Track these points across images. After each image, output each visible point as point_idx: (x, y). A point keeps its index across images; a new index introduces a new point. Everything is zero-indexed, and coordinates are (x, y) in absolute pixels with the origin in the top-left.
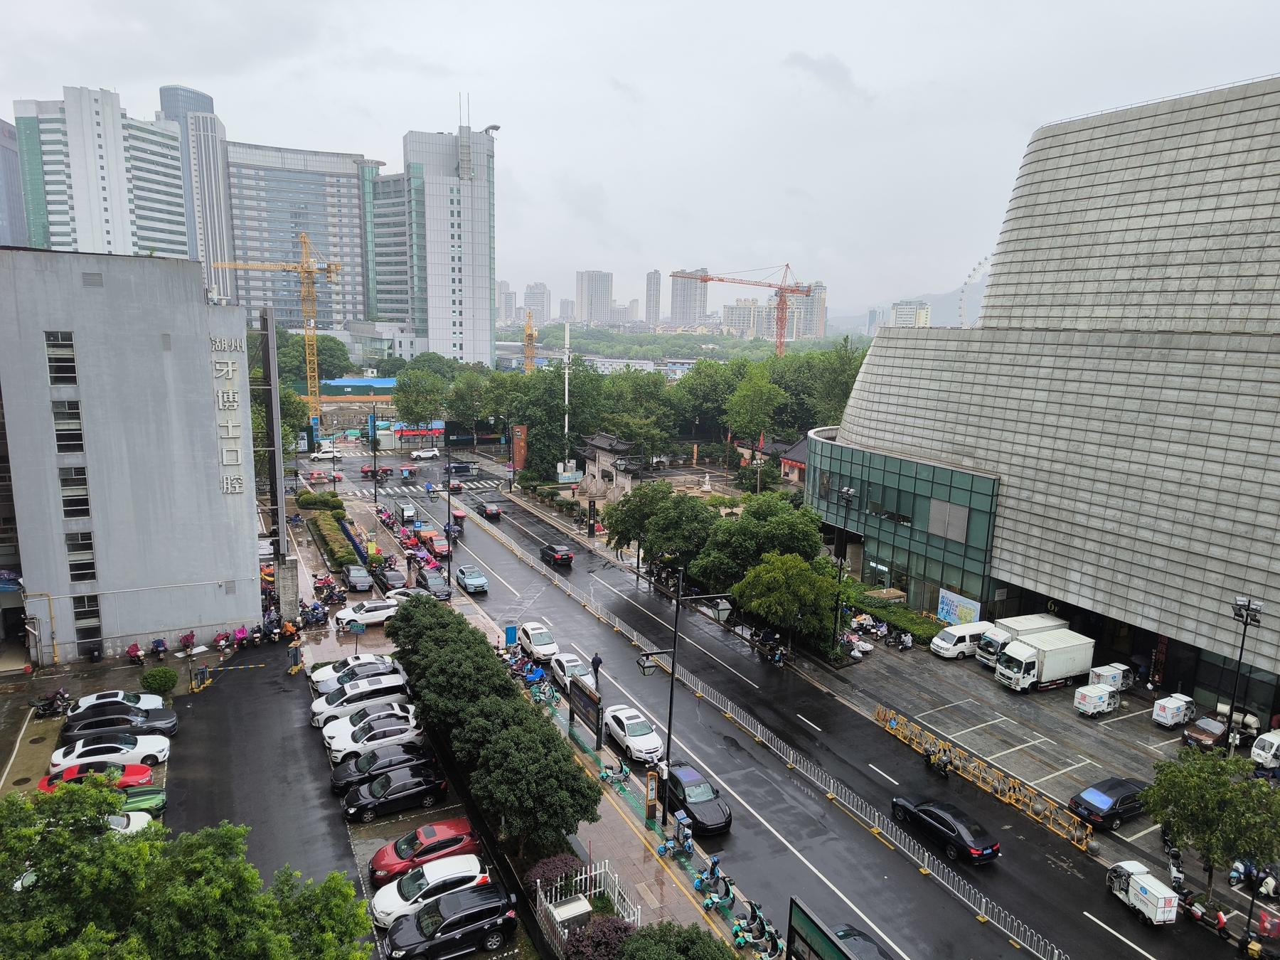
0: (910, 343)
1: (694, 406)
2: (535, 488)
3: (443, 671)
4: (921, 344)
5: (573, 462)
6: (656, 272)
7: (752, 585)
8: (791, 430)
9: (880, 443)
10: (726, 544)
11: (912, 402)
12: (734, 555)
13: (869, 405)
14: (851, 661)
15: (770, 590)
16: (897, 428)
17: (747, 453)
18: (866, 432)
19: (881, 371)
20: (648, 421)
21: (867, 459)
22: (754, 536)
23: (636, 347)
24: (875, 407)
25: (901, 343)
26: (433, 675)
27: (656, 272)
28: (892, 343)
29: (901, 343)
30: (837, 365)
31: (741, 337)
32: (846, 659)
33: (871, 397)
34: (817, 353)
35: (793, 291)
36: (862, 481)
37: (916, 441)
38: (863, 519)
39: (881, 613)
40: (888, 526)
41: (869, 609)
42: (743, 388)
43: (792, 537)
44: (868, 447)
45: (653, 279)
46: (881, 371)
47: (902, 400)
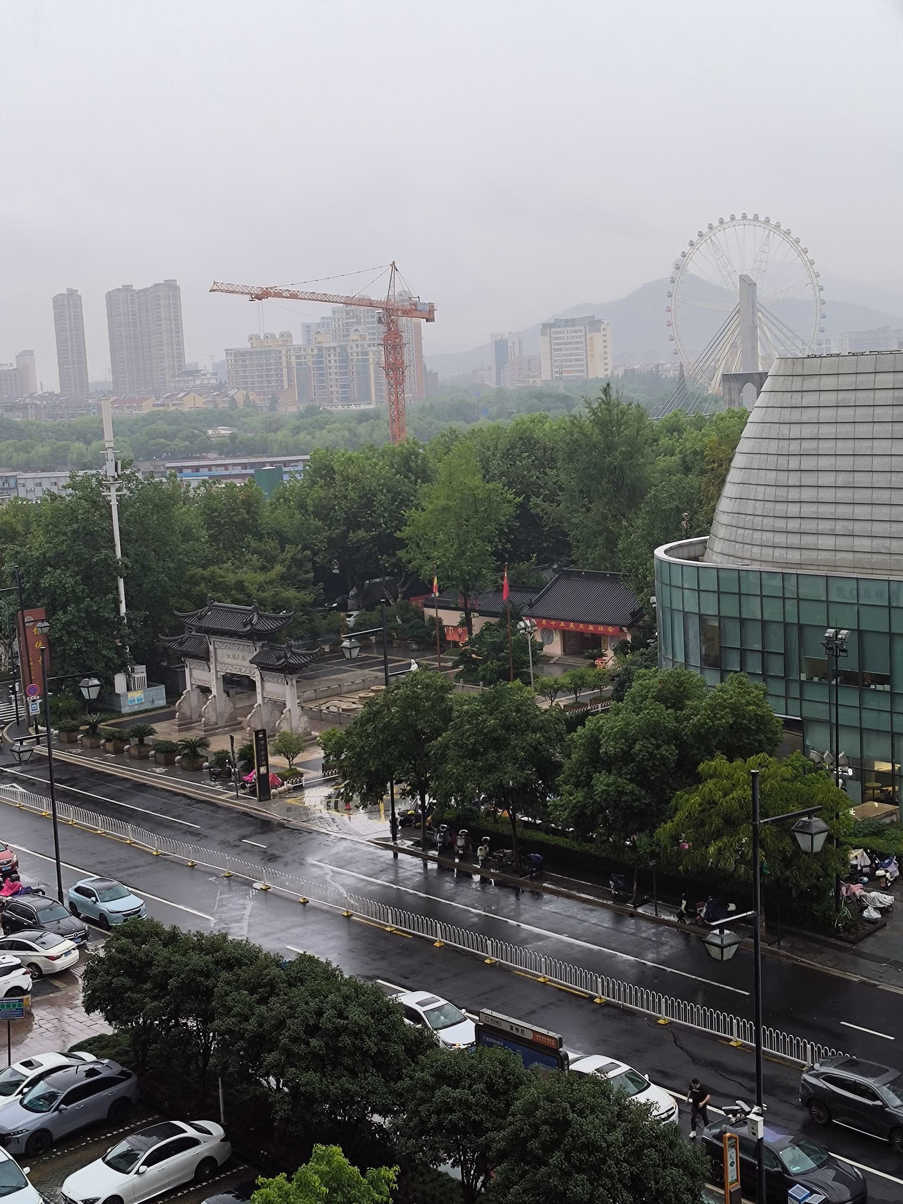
0: (846, 382)
1: (330, 540)
2: (94, 726)
3: (313, 1030)
4: (865, 381)
5: (140, 672)
6: (72, 293)
7: (698, 822)
8: (524, 566)
9: (813, 555)
10: (626, 757)
11: (862, 479)
12: (641, 777)
13: (781, 493)
14: (869, 927)
15: (730, 823)
16: (840, 527)
17: (451, 618)
18: (780, 539)
19: (795, 431)
20: (273, 574)
21: (787, 585)
22: (675, 737)
23: (78, 445)
24: (793, 494)
25: (829, 383)
26: (295, 1040)
27: (72, 293)
28: (812, 384)
29: (829, 383)
30: (596, 436)
31: (272, 408)
32: (856, 930)
33: (782, 478)
34: (557, 417)
35: (406, 313)
36: (786, 625)
37: (878, 544)
38: (795, 692)
39: (879, 843)
40: (848, 697)
41: (855, 841)
42: (433, 499)
43: (735, 729)
44: (788, 564)
45: (67, 308)
46: (795, 431)
47: (842, 479)
